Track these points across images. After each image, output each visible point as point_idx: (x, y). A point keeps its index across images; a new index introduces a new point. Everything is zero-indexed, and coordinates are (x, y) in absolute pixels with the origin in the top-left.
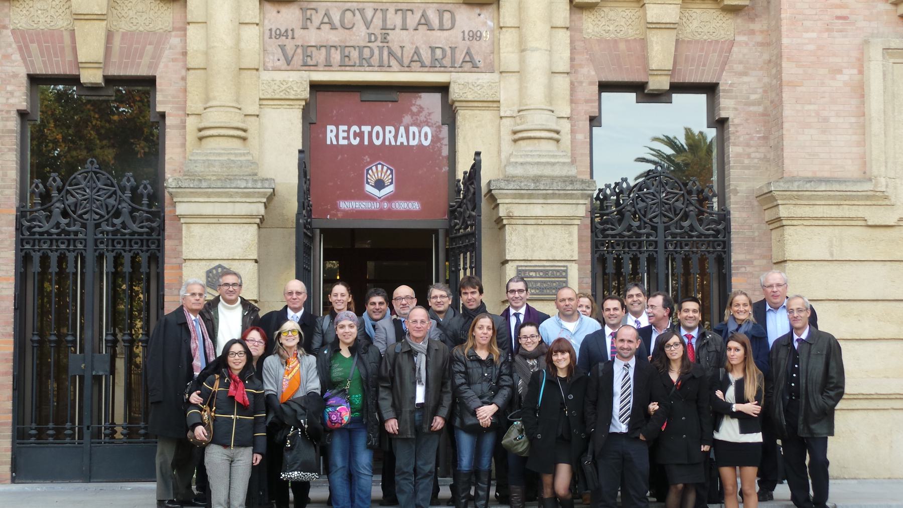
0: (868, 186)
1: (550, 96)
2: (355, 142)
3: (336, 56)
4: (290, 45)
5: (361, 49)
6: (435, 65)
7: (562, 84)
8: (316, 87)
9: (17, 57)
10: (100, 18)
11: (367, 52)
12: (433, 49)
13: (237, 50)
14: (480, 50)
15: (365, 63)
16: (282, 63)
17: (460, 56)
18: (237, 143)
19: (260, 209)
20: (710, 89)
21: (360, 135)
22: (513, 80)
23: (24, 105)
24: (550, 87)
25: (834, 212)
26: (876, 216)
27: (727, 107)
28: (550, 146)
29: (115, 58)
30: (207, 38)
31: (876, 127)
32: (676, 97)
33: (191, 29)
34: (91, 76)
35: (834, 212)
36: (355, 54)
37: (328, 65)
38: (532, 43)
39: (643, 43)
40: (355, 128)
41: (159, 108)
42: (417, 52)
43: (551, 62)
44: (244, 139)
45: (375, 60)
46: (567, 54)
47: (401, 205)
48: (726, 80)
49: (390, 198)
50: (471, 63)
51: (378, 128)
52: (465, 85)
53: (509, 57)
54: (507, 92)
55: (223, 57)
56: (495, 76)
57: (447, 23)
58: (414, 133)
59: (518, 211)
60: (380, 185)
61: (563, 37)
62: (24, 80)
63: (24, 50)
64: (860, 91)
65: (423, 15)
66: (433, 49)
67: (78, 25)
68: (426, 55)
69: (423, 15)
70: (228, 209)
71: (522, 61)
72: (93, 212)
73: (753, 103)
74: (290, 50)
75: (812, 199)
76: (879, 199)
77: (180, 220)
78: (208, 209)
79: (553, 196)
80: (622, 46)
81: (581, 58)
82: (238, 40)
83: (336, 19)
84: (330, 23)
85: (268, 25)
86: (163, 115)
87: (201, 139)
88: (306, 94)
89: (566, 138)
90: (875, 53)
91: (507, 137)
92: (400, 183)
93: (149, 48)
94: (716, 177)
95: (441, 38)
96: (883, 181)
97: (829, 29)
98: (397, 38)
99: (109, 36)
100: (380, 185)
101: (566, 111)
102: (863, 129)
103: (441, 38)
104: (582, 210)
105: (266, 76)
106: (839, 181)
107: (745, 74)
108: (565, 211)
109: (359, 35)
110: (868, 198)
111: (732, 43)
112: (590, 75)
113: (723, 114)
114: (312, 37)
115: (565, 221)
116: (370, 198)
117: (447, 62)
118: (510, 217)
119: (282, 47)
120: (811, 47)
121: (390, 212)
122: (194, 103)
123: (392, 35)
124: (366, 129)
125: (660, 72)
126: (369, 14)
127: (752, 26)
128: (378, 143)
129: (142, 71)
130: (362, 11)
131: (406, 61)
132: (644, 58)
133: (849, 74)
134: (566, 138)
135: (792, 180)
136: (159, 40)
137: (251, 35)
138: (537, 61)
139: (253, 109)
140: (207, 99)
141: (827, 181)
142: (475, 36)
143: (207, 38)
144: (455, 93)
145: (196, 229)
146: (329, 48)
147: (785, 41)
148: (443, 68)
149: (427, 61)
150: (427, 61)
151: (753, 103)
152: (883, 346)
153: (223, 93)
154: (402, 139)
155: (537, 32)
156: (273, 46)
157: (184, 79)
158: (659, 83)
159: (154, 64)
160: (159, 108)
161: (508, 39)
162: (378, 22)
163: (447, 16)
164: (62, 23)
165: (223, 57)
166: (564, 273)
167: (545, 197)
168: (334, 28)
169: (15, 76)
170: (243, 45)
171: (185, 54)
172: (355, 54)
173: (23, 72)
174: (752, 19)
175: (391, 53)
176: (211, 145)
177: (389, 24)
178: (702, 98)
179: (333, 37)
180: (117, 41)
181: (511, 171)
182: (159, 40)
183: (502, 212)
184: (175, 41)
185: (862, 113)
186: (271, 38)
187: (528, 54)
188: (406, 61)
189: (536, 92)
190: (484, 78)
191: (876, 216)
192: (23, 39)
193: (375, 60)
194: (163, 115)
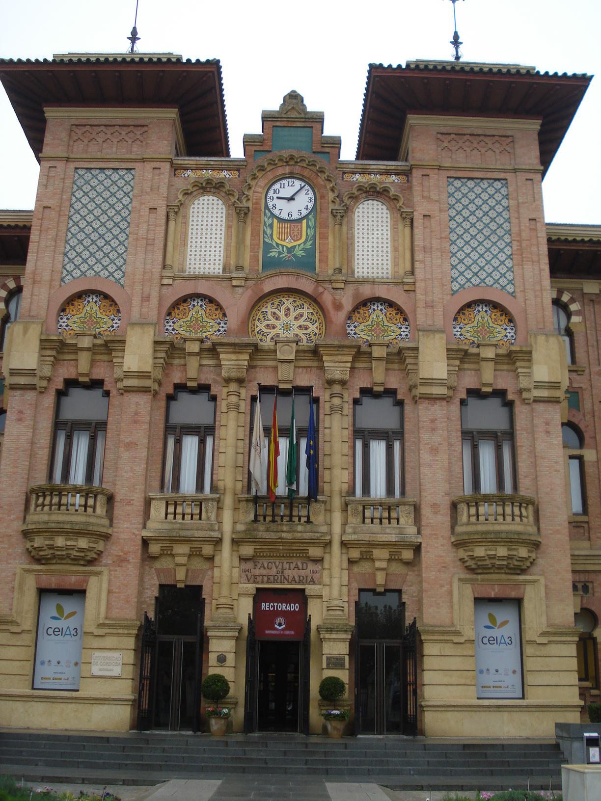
0: (454, 629)
1: (340, 595)
2: (272, 609)
3: (265, 579)
4: (249, 575)
5: (274, 576)
6: (300, 582)
7: (345, 589)
8: (258, 589)
9: (156, 578)
10: (184, 565)
11: (276, 577)
12: (299, 576)
13: (231, 576)
14: (316, 577)
15: (275, 582)
16: (246, 581)
17: (309, 579)
18: (229, 611)
19: (237, 634)
21: (274, 606)
22: (327, 587)
23: (157, 595)
24: (340, 591)
25: (442, 638)
26: (456, 639)
27: (405, 599)
28: (340, 613)
29: (189, 579)
30: (221, 572)
31: (456, 607)
32: (387, 594)
33: (215, 569)
34: (180, 585)
35: (442, 638)
36: (272, 578)
37: (262, 582)
38: (334, 575)
39: (374, 575)
40: (272, 604)
41: (203, 597)
42: (294, 577)
43: (341, 582)
44: (232, 608)
45: (279, 581)
46: (347, 578)
47: (287, 632)
48: (404, 589)
49: (283, 630)
50: (313, 582)
51: (280, 604)
52: (311, 589)
53: (326, 580)
54: (325, 592)
55: (226, 579)
56: (321, 587)
57: (305, 567)
58: (100, 670)
59: (327, 636)
60: (280, 625)
61: (346, 572)
62: (158, 586)
63: (158, 576)
64: (451, 593)
65: (296, 564)
66: (299, 576)
67: (177, 568)
68: (297, 579)
69: (296, 564)
70: (226, 634)
71: (331, 581)
73: (414, 597)
74: (249, 577)
75: (433, 633)
76: (458, 633)
77: (111, 354)
79: (339, 631)
80: (367, 575)
82: (231, 572)
83: (266, 565)
84: (264, 567)
85: (242, 567)
86: (204, 599)
87: (217, 608)
88: (255, 592)
89: (346, 609)
90: (456, 580)
91: (325, 609)
92: (286, 623)
93: (201, 575)
94: (171, 636)
95: (302, 573)
96: (458, 626)
97: (439, 571)
98: (287, 572)
99: (187, 570)
100: (280, 625)
101: (346, 600)
103: (302, 573)
104: (577, 639)
105: (241, 585)
106: (443, 627)
107: (412, 586)
108: (344, 636)
110: (453, 633)
111: (407, 574)
112: (355, 586)
113: (404, 601)
114: (257, 572)
115: (344, 640)
116: (277, 629)
117: (304, 581)
118: (324, 638)
119: (247, 575)
120: (433, 577)
121: (284, 635)
122: (215, 595)
123: (285, 572)
124: (276, 604)
125: (380, 585)
126: (277, 564)
127: (414, 568)
128: (280, 609)
129: (198, 583)
130: (275, 563)
131: (290, 581)
132: (375, 580)
133: (447, 587)
134: (346, 609)
135: (426, 625)
137: (236, 571)
138: (336, 582)
139: (236, 597)
140: (220, 594)
141: (439, 626)
142: (314, 572)
143: (221, 572)
144: (307, 592)
145: (214, 641)
146: (263, 576)
147: (424, 575)
148: (303, 583)
149: (297, 581)
150: (297, 581)
151: (414, 597)
152: (459, 687)
153: (225, 591)
154: (288, 608)
155: (336, 571)
156: (243, 575)
157: (212, 586)
159: (202, 581)
160: (203, 597)
161: (326, 573)
162: (280, 567)
163: (305, 564)
165: (226, 579)
166: (343, 659)
167: (337, 631)
168: (265, 569)
169: (155, 584)
170: (233, 574)
171: (213, 577)
172: (272, 578)
173: (158, 583)
174: (414, 566)
175: (284, 578)
176: (221, 610)
177: (284, 567)
178: (397, 594)
179: (264, 572)
180: (190, 574)
181: (325, 621)
183: (322, 636)
184: (210, 573)
185: (451, 601)
187: (333, 579)
188: (290, 581)
189: (335, 594)
190: (317, 587)
191: (456, 639)
193: (279, 581)
194: (204, 599)
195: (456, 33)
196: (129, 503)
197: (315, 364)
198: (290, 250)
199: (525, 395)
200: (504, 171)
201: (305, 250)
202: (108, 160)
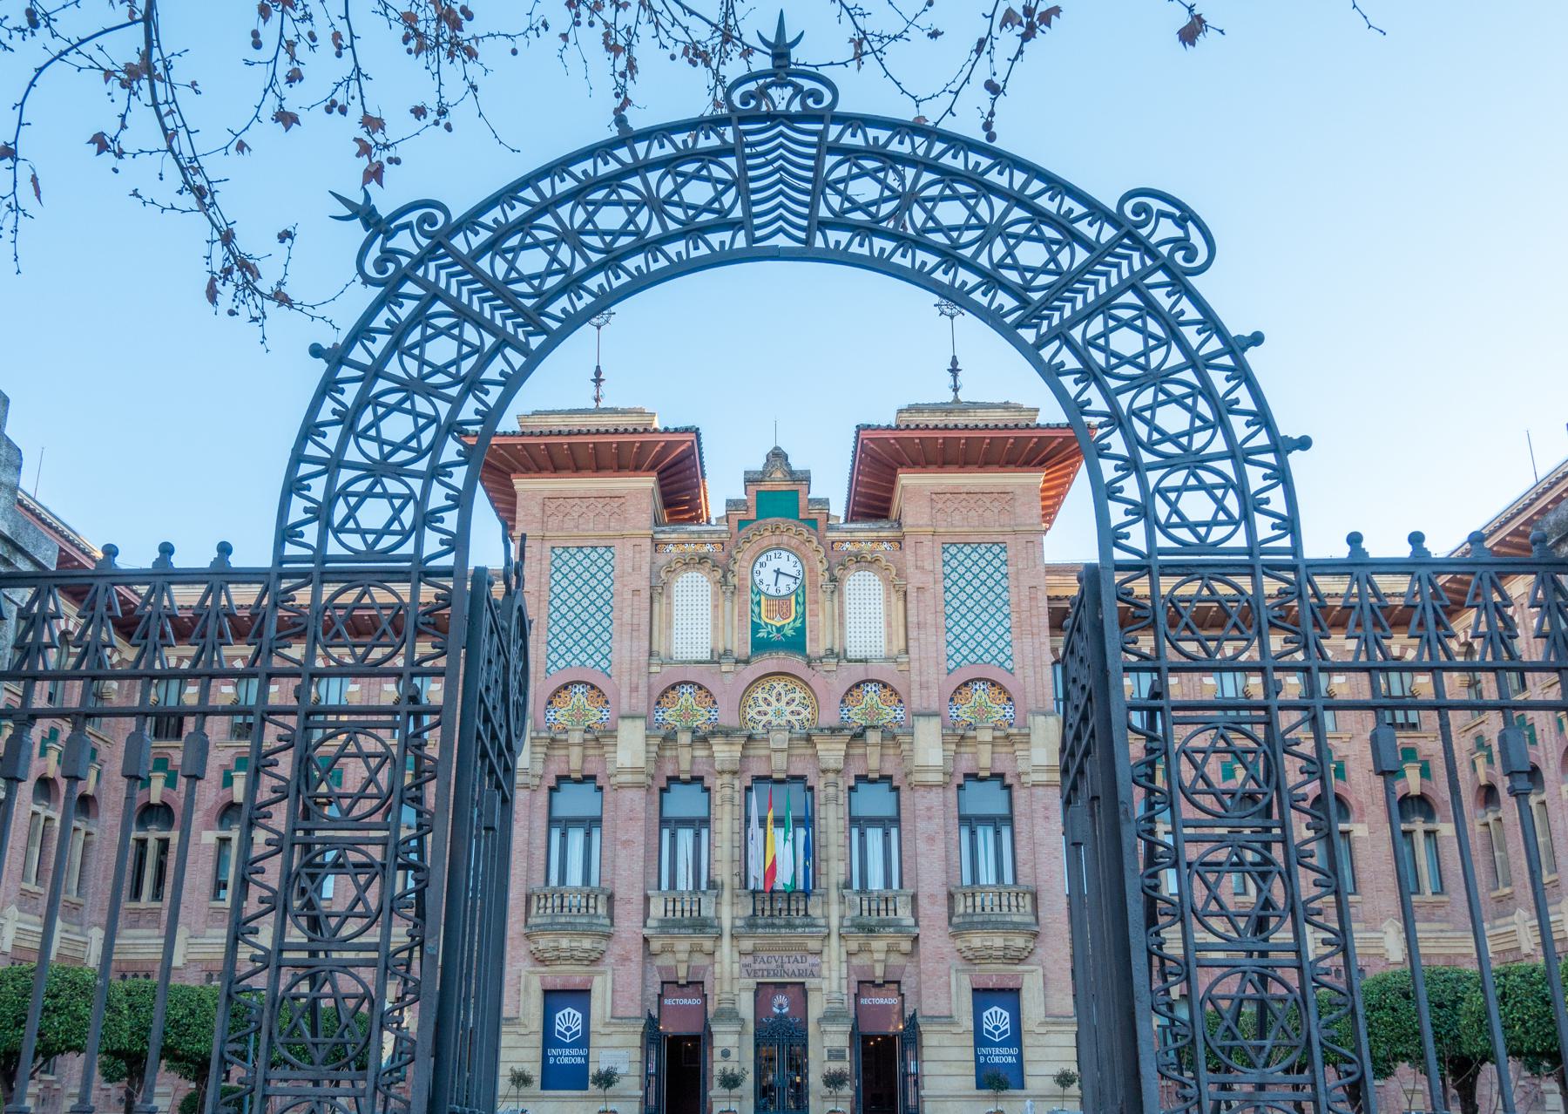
1: (840, 987)
6: (800, 975)
7: (844, 982)
8: (758, 984)
14: (815, 969)
15: (775, 975)
20: (898, 983)
26: (954, 1029)
31: (954, 998)
48: (903, 980)
53: (825, 973)
61: (844, 965)
63: (660, 973)
72: (1202, 869)
78: (723, 1029)
81: (851, 972)
95: (802, 966)
98: (787, 966)
102: (950, 998)
105: (742, 981)
109: (774, 965)
114: (757, 966)
115: (635, 1032)
122: (717, 991)
136: (705, 968)
137: (736, 966)
144: (807, 986)
153: (727, 988)
156: (744, 970)
158: (880, 981)
161: (825, 966)
164: (673, 963)
165: (727, 975)
182: (705, 968)
185: (949, 992)
186: (1049, 599)
189: (835, 987)
192: (660, 969)
195: (598, 367)
196: (629, 902)
197: (810, 751)
198: (779, 630)
199: (1024, 779)
200: (1003, 533)
201: (795, 629)
202: (586, 537)
